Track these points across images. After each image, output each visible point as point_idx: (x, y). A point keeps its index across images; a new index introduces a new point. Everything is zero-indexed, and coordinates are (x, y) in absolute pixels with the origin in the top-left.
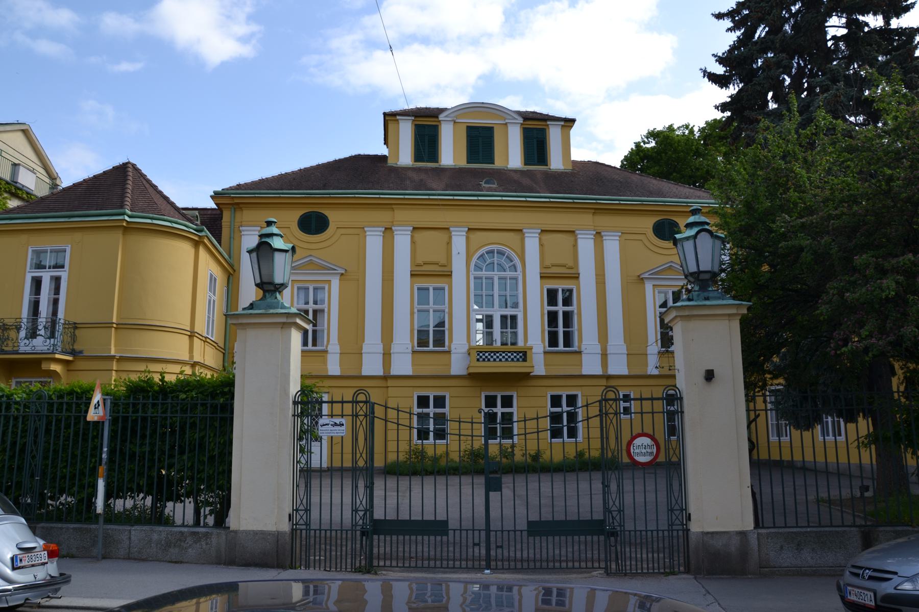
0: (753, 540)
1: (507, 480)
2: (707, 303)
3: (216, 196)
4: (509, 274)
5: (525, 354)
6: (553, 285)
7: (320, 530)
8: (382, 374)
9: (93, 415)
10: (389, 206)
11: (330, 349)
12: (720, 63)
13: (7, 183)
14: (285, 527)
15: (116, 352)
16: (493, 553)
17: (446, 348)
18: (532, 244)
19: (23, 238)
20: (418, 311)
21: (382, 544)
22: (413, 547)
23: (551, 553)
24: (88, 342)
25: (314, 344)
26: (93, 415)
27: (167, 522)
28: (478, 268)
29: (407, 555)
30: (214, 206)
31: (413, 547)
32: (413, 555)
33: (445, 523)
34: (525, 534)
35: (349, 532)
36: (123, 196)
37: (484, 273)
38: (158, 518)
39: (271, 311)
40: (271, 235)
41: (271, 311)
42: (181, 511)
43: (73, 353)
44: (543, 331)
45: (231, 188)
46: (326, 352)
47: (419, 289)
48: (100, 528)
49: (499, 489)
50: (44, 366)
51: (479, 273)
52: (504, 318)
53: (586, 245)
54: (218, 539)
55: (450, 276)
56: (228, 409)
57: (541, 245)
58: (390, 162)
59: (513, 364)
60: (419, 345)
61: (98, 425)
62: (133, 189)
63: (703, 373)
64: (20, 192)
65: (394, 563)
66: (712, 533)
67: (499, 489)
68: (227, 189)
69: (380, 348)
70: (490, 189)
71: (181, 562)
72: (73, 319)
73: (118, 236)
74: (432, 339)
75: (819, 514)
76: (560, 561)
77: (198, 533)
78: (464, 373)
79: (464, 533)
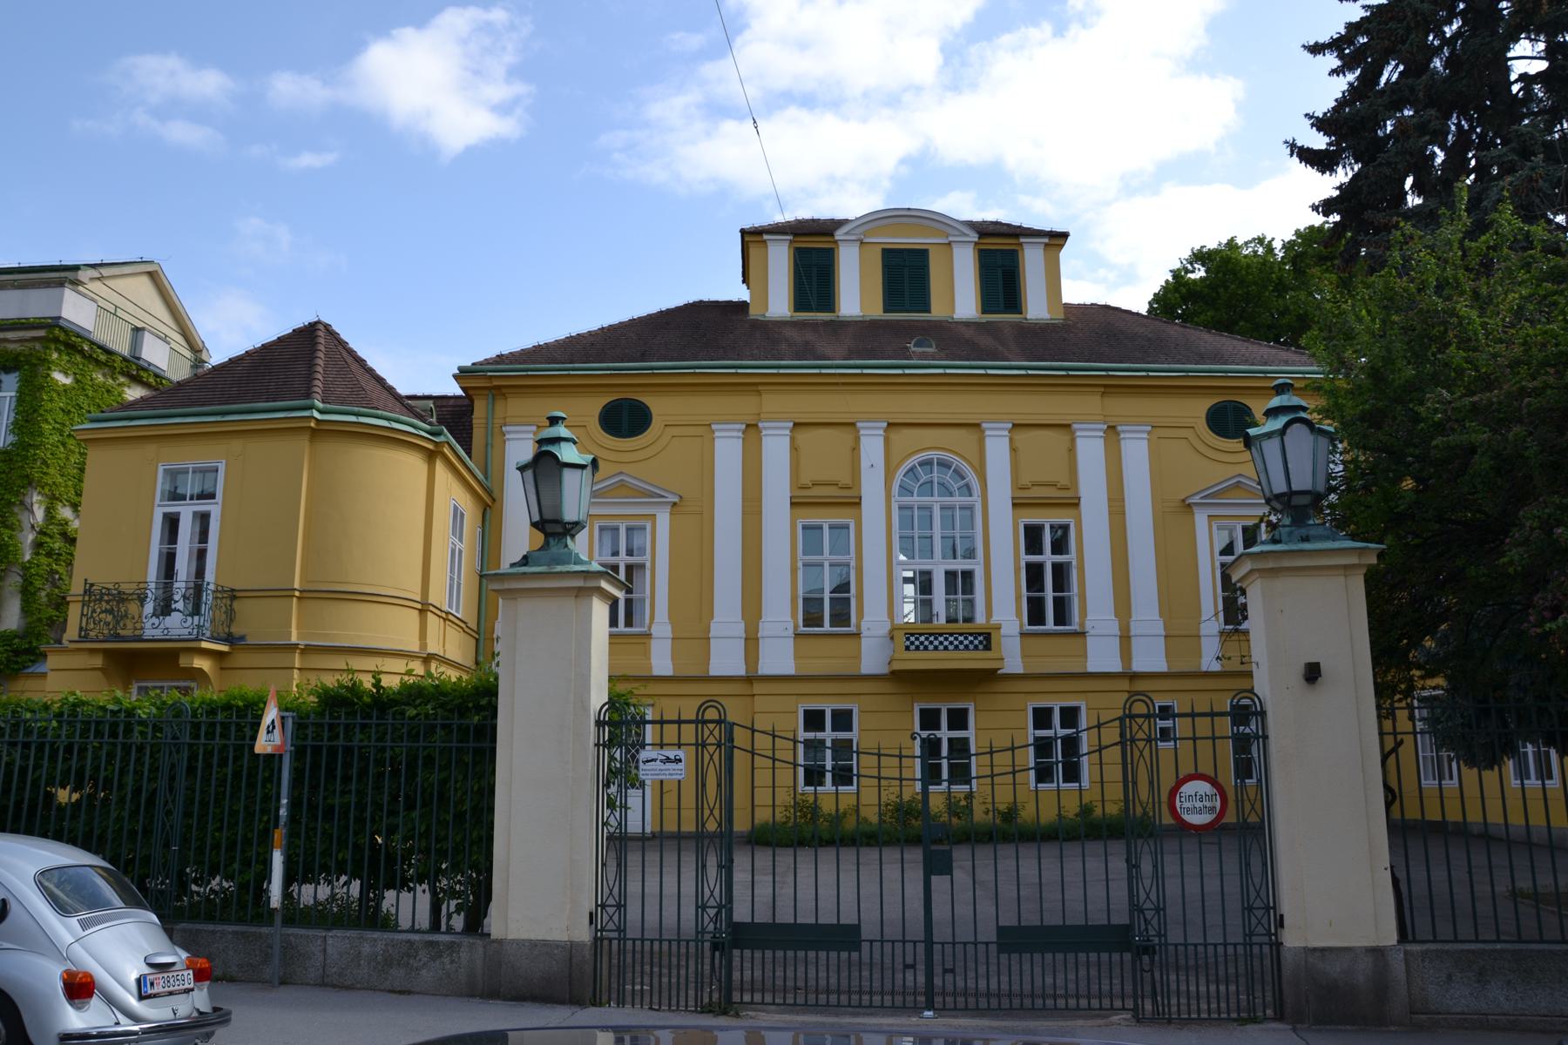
1: (961, 855)
2: (1307, 546)
3: (463, 375)
4: (958, 500)
5: (988, 637)
6: (1034, 517)
7: (643, 940)
8: (742, 672)
9: (265, 743)
10: (752, 387)
12: (1319, 130)
13: (125, 359)
14: (584, 934)
16: (938, 981)
17: (852, 629)
18: (997, 448)
19: (151, 449)
20: (804, 565)
21: (747, 965)
24: (254, 621)
25: (629, 623)
26: (265, 743)
27: (382, 922)
28: (905, 490)
29: (790, 983)
30: (460, 392)
31: (801, 969)
32: (801, 983)
33: (855, 929)
34: (993, 948)
36: (309, 378)
37: (915, 500)
38: (370, 917)
39: (559, 568)
40: (557, 440)
41: (559, 568)
42: (409, 906)
43: (229, 639)
44: (1018, 598)
45: (487, 362)
46: (648, 636)
47: (804, 528)
48: (275, 933)
49: (947, 870)
51: (907, 500)
52: (950, 575)
53: (1090, 449)
54: (471, 954)
58: (754, 312)
59: (967, 654)
60: (807, 623)
61: (272, 760)
66: (1323, 950)
67: (947, 870)
68: (481, 363)
69: (740, 629)
70: (923, 356)
71: (409, 992)
72: (229, 584)
73: (303, 444)
74: (828, 612)
76: (1055, 997)
77: (437, 943)
78: (884, 670)
79: (887, 947)
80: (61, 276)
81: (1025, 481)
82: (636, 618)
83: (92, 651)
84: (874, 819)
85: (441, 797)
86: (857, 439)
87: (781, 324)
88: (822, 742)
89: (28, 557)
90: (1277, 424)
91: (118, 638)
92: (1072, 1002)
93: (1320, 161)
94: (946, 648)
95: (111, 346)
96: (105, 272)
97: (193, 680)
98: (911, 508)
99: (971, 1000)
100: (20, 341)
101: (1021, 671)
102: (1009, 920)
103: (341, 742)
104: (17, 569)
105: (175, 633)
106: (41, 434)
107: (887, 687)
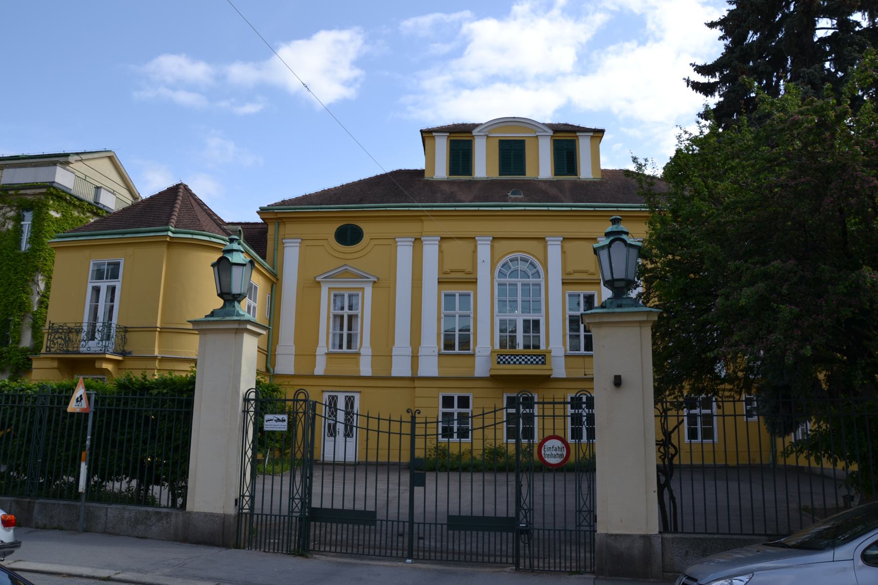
0: (657, 544)
1: (430, 478)
2: (619, 310)
3: (262, 211)
4: (532, 280)
7: (262, 515)
8: (410, 375)
9: (73, 407)
10: (418, 218)
11: (362, 352)
12: (698, 72)
13: (90, 204)
14: (231, 510)
15: (159, 353)
16: (415, 544)
17: (471, 352)
18: (554, 251)
19: (87, 252)
20: (445, 316)
21: (316, 529)
22: (372, 536)
23: (492, 548)
24: (136, 344)
25: (349, 347)
26: (73, 407)
27: (152, 502)
28: (502, 274)
29: (355, 542)
30: (260, 221)
31: (372, 536)
32: (361, 543)
33: (374, 513)
34: (445, 527)
35: (286, 518)
36: (170, 215)
37: (507, 280)
38: (141, 498)
39: (228, 318)
40: (231, 251)
41: (228, 318)
42: (160, 493)
43: (123, 353)
44: (564, 336)
45: (276, 204)
46: (358, 354)
47: (446, 295)
48: (82, 504)
49: (423, 484)
50: (97, 365)
51: (503, 280)
52: (526, 322)
54: (177, 518)
55: (475, 282)
56: (190, 403)
57: (563, 252)
58: (427, 176)
59: (532, 367)
61: (81, 417)
62: (181, 207)
63: (612, 378)
64: (100, 212)
65: (333, 549)
66: (616, 535)
67: (423, 484)
68: (272, 205)
69: (409, 351)
70: (515, 200)
71: (146, 538)
72: (123, 324)
73: (163, 249)
74: (457, 343)
75: (789, 522)
76: (495, 556)
77: (160, 513)
78: (488, 375)
79: (427, 526)
80: (61, 159)
81: (569, 270)
82: (353, 344)
83: (52, 359)
84: (479, 457)
85: (169, 438)
86: (476, 246)
87: (441, 182)
88: (452, 414)
89: (35, 309)
90: (606, 241)
91: (68, 352)
92: (492, 559)
93: (706, 89)
94: (520, 363)
95: (81, 196)
96: (84, 157)
97: (104, 375)
98: (529, 285)
99: (433, 554)
100: (34, 194)
101: (564, 376)
102: (454, 511)
103: (121, 407)
104: (30, 315)
105: (93, 350)
106: (43, 244)
107: (489, 384)
